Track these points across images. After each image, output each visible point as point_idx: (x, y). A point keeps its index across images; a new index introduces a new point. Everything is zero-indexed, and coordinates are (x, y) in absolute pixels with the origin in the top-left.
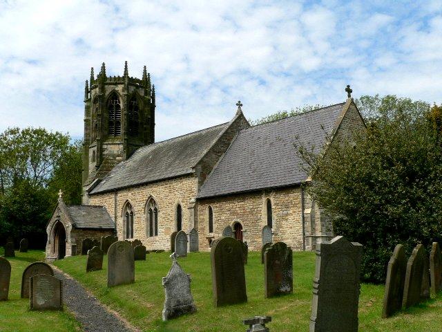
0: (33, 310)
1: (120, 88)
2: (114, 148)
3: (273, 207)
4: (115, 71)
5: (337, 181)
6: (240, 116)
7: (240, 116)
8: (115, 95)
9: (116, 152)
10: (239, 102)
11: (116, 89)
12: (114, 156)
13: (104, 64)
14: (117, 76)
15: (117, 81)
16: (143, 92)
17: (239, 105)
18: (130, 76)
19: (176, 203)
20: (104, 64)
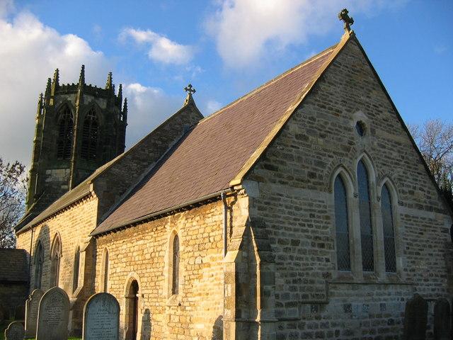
0: (349, 266)
1: (71, 98)
2: (60, 174)
3: (181, 248)
4: (66, 80)
5: (444, 274)
6: (191, 103)
7: (191, 103)
8: (67, 108)
9: (61, 180)
10: (190, 86)
11: (69, 99)
12: (59, 184)
13: (57, 70)
14: (66, 85)
15: (71, 89)
16: (105, 104)
17: (190, 89)
18: (87, 83)
19: (75, 245)
20: (57, 70)
